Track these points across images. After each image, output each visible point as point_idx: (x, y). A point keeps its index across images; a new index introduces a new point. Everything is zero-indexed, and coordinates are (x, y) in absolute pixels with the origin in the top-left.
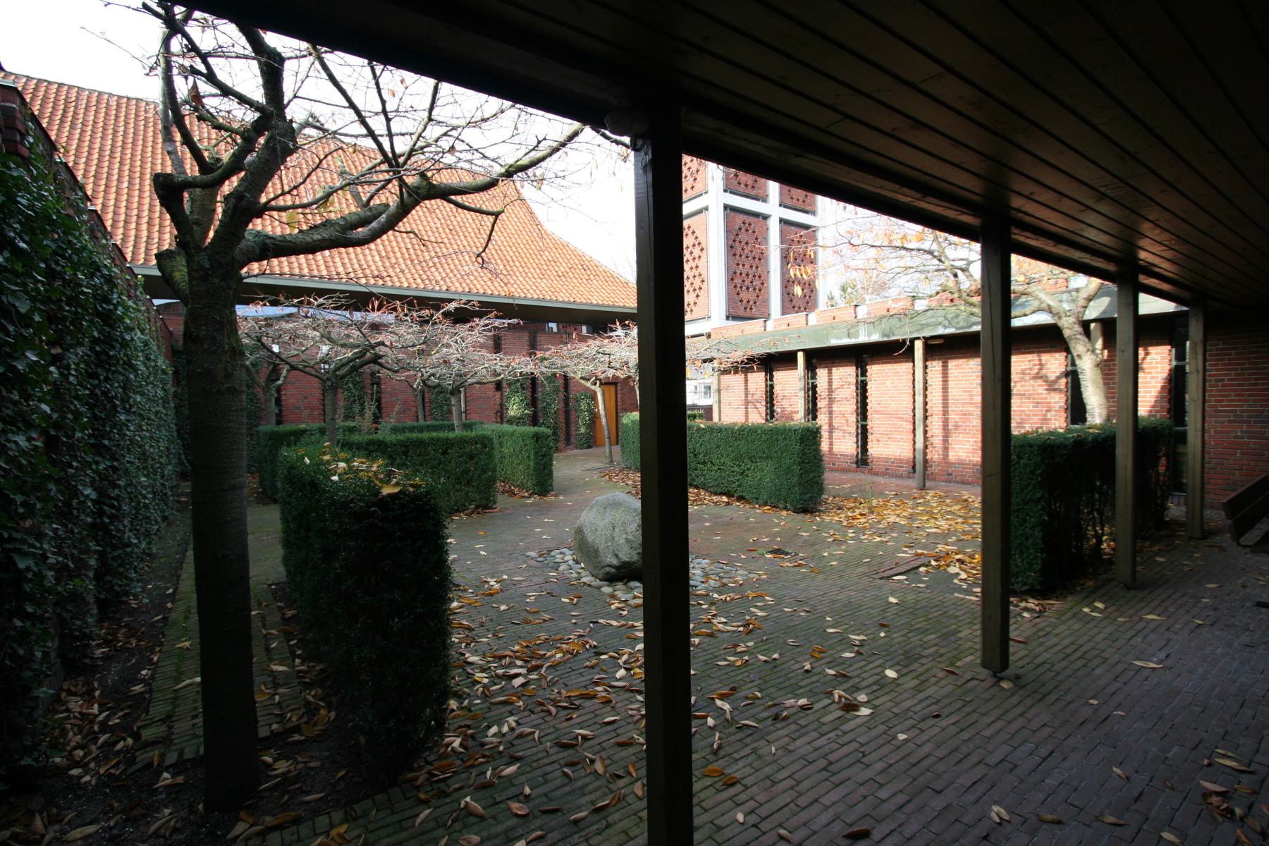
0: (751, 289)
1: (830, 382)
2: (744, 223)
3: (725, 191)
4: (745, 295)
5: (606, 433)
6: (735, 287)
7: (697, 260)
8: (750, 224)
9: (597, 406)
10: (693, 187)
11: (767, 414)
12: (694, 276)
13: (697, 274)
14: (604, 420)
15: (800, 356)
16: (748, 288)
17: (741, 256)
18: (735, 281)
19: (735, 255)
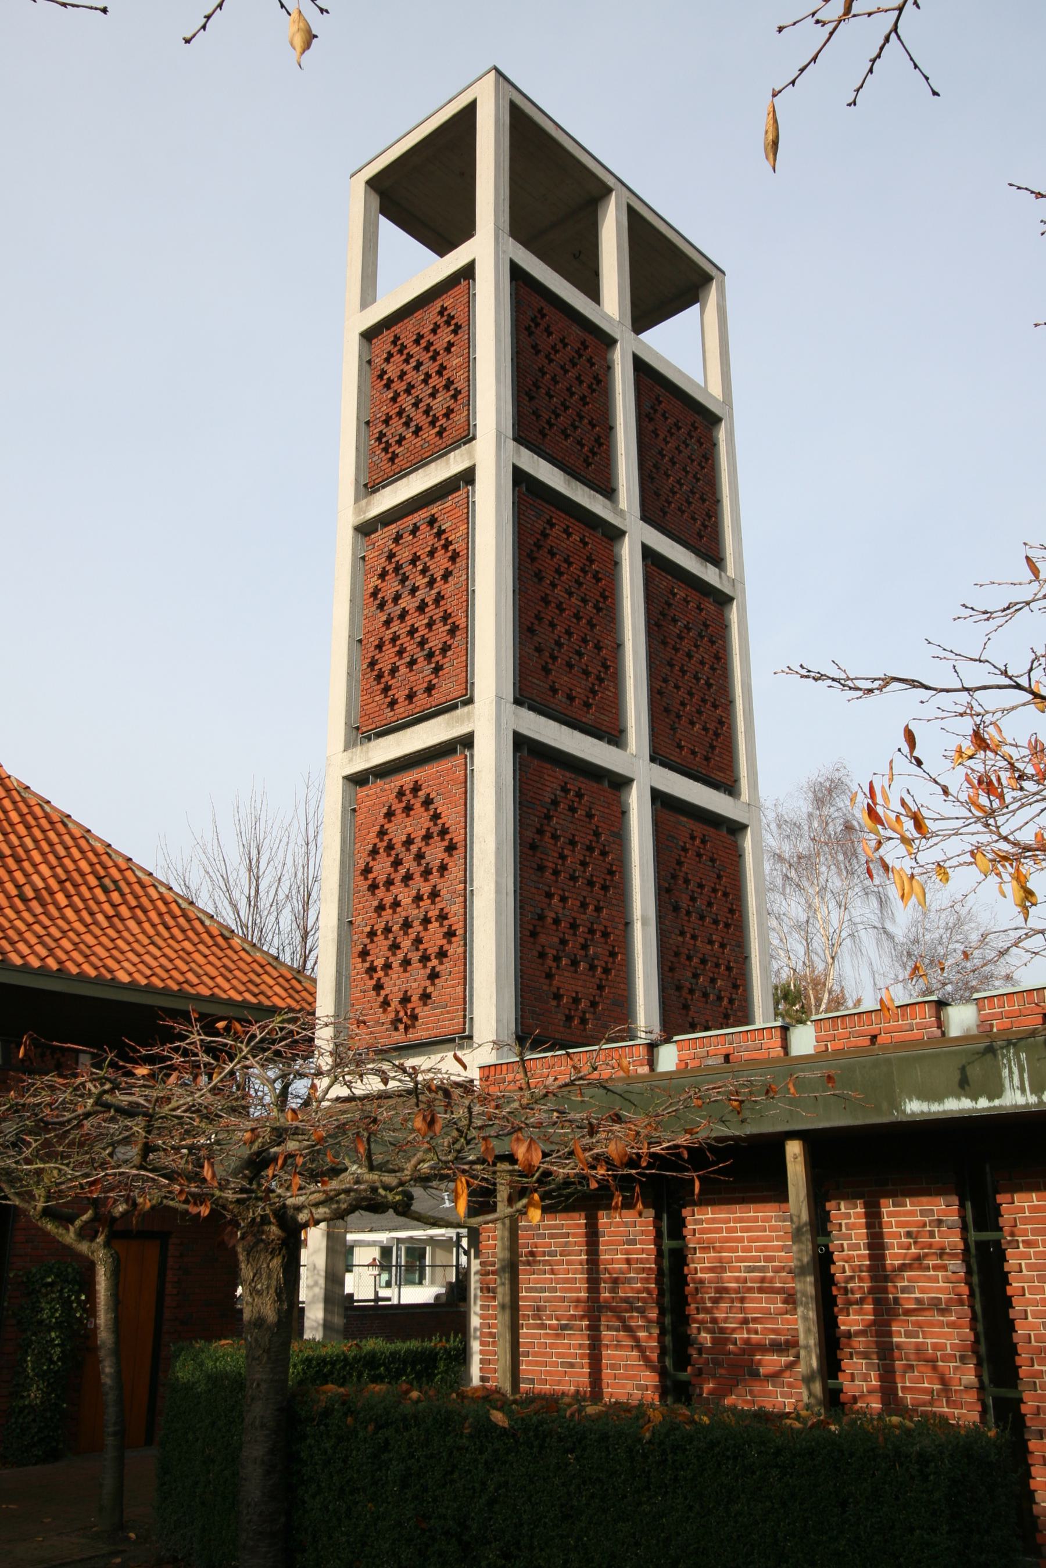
0: (582, 966)
1: (876, 1244)
2: (565, 790)
3: (517, 702)
4: (567, 982)
5: (111, 1413)
6: (542, 955)
7: (380, 927)
8: (579, 795)
9: (92, 1312)
10: (430, 689)
11: (663, 1352)
12: (426, 921)
13: (433, 913)
14: (108, 1368)
15: (794, 1149)
16: (575, 963)
17: (556, 873)
18: (542, 939)
19: (541, 868)
